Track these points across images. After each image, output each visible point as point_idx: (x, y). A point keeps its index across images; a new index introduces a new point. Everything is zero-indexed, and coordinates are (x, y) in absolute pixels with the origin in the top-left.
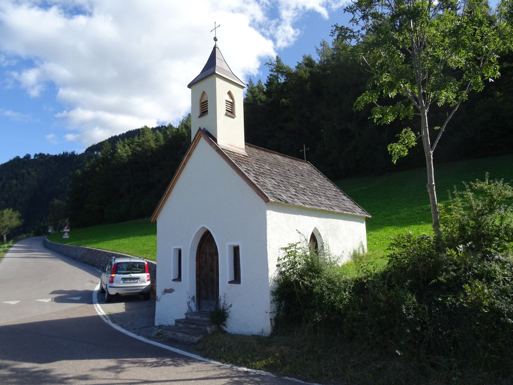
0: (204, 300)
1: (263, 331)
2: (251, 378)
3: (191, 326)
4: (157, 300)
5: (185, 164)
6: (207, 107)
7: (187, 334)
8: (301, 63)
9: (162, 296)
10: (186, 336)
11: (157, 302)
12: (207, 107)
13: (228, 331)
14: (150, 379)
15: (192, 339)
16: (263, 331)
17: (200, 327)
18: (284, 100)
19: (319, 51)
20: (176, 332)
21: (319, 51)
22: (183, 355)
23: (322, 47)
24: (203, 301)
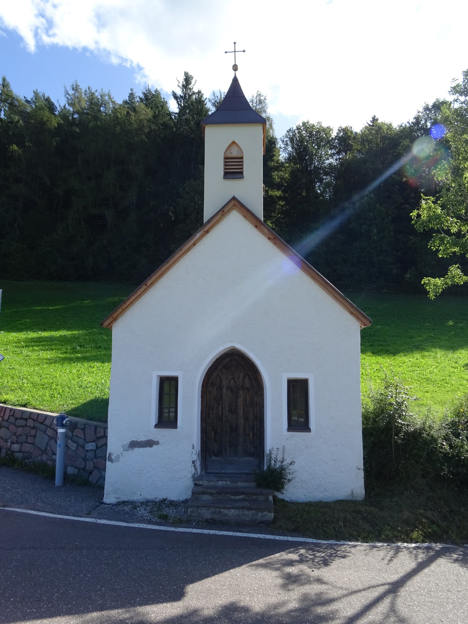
0: (214, 456)
1: (353, 493)
2: (302, 551)
3: (233, 497)
4: (111, 460)
5: (194, 244)
6: (241, 163)
7: (250, 509)
8: (29, 99)
9: (125, 452)
10: (246, 512)
11: (108, 463)
12: (241, 163)
13: (286, 499)
14: (355, 588)
15: (261, 516)
16: (353, 493)
17: (254, 497)
18: (15, 147)
19: (69, 95)
20: (224, 508)
21: (69, 95)
22: (300, 542)
23: (73, 92)
24: (211, 457)
